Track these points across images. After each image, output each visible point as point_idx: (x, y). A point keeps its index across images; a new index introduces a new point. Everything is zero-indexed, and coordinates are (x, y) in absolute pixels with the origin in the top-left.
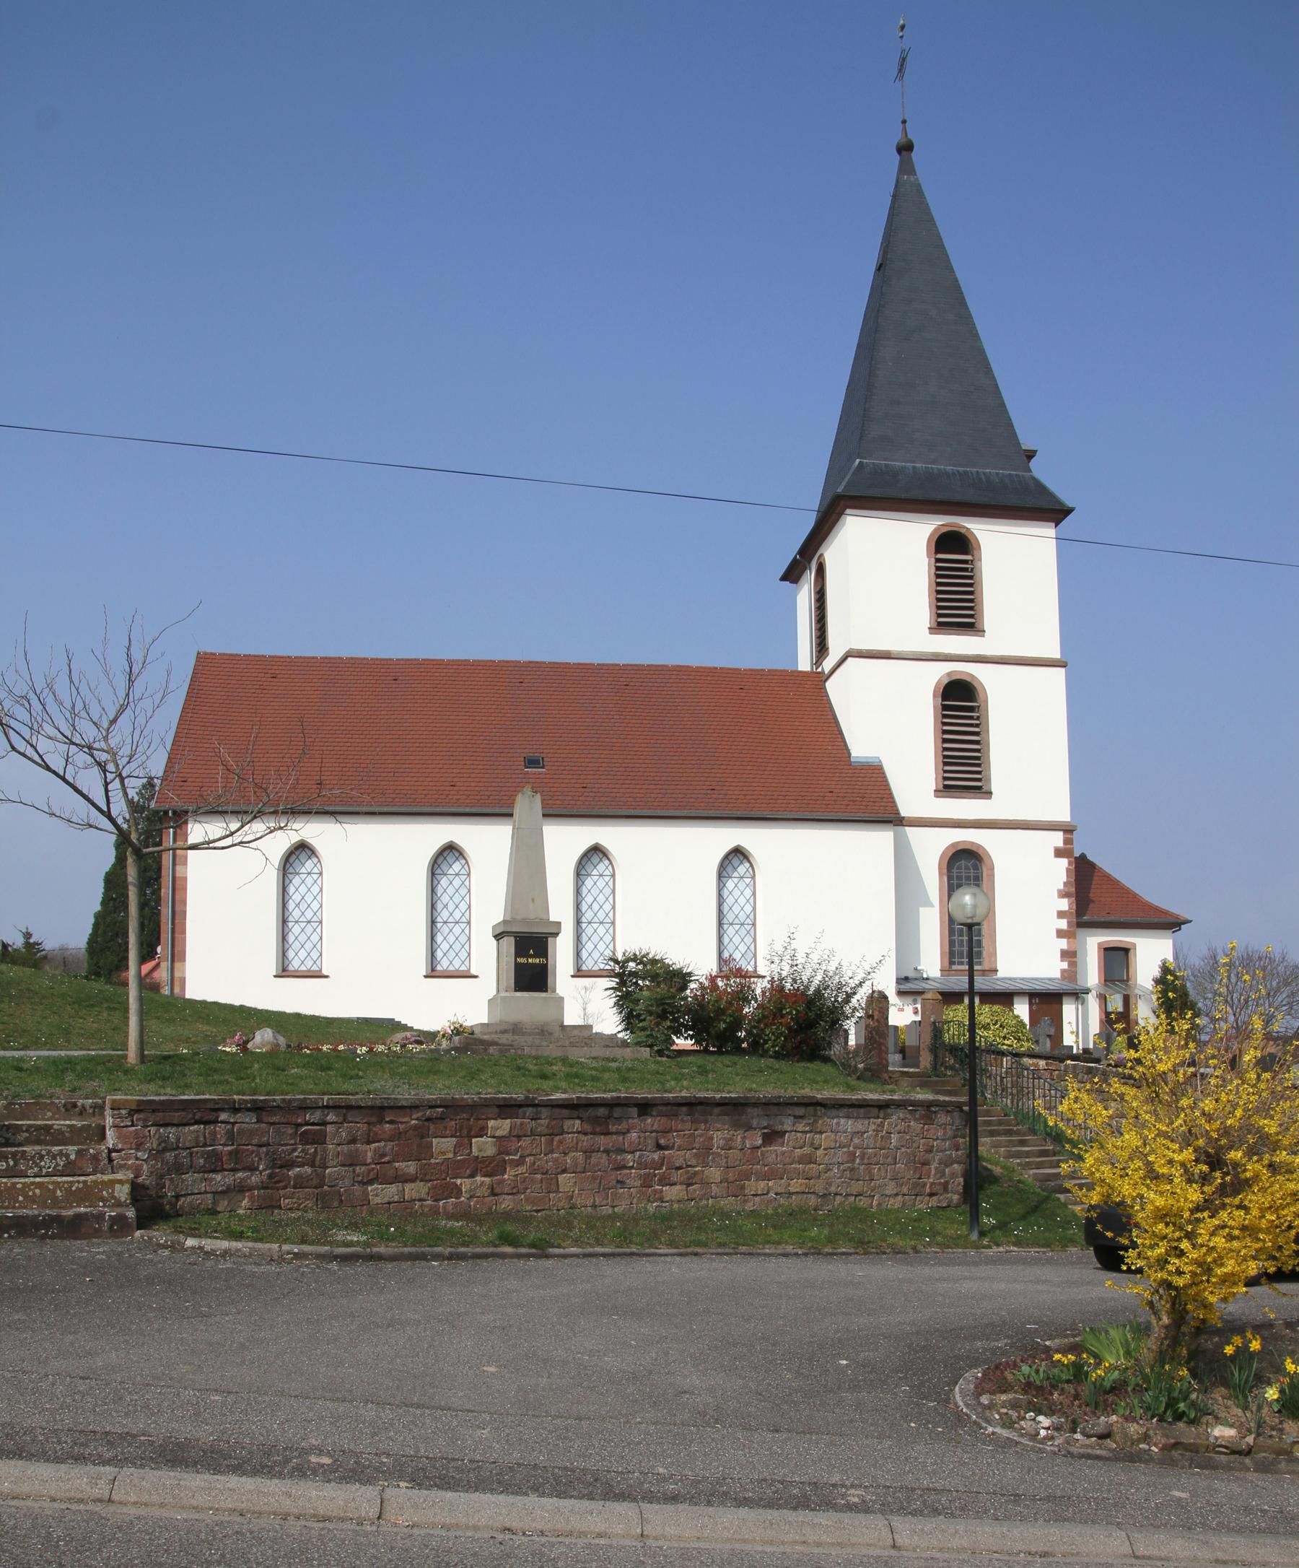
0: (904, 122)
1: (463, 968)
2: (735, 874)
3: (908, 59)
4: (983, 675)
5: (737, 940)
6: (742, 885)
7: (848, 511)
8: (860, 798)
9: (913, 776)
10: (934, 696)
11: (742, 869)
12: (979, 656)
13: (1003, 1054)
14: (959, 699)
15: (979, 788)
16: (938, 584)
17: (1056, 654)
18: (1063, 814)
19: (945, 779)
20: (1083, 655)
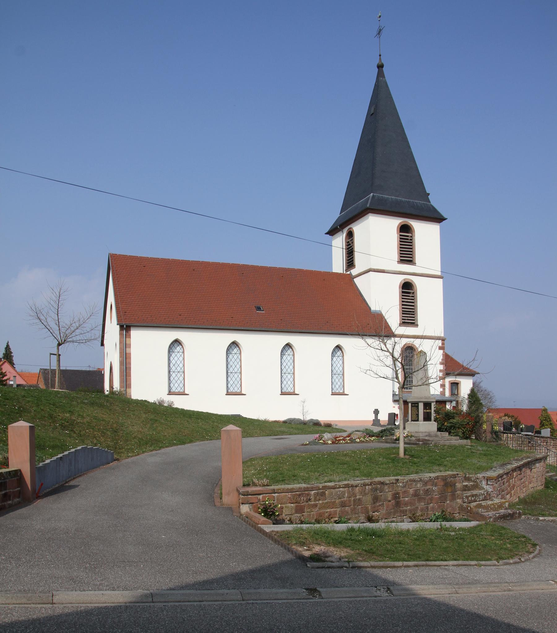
0: (380, 55)
1: (341, 391)
3: (383, 31)
4: (415, 280)
5: (337, 380)
6: (338, 359)
8: (372, 326)
9: (393, 318)
14: (407, 288)
15: (414, 323)
16: (401, 245)
17: (439, 273)
18: (440, 332)
19: (403, 319)
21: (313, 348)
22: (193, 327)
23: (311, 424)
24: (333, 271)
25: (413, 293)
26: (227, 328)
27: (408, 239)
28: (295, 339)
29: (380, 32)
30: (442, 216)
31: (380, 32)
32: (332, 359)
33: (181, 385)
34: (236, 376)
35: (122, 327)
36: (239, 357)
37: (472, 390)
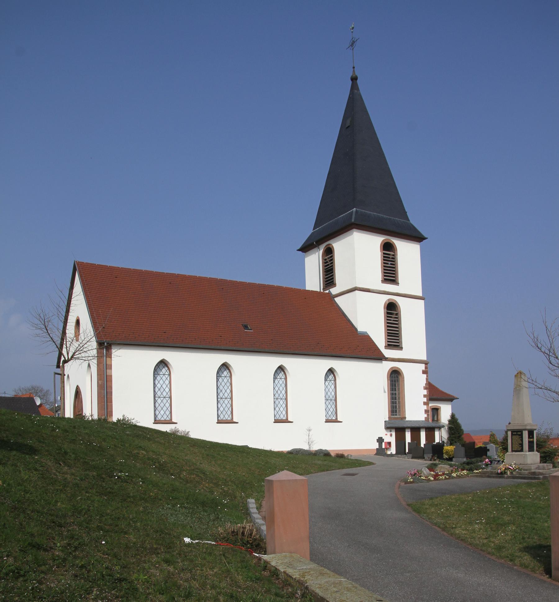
0: (354, 68)
1: (334, 418)
4: (400, 301)
6: (331, 384)
11: (226, 373)
12: (384, 291)
14: (392, 309)
17: (420, 294)
19: (388, 342)
20: (432, 294)
21: (308, 371)
22: (181, 346)
23: (322, 455)
24: (307, 289)
25: (397, 314)
26: (218, 347)
27: (389, 258)
28: (288, 362)
29: (353, 44)
30: (423, 236)
31: (353, 44)
32: (155, 379)
33: (168, 413)
34: (226, 402)
35: (100, 344)
36: (229, 380)
37: (453, 416)
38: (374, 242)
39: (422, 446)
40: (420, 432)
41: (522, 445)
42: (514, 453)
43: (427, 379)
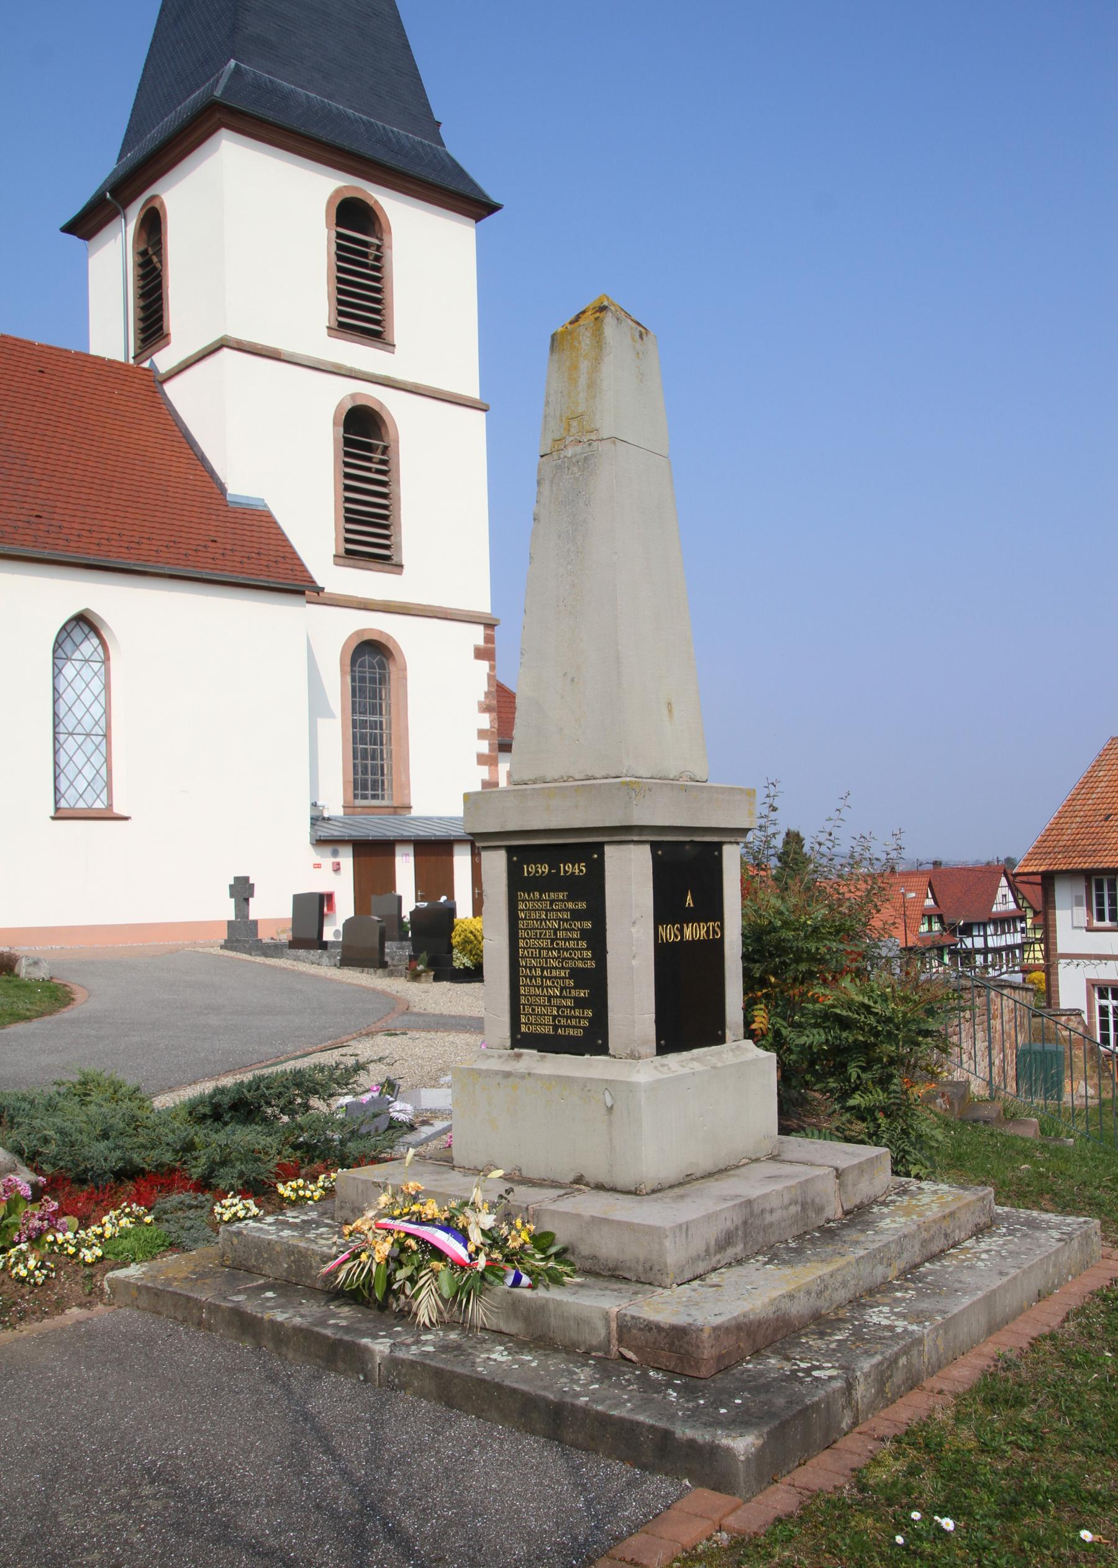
1: (99, 805)
2: (77, 655)
4: (397, 408)
5: (79, 759)
6: (87, 673)
7: (224, 132)
9: (312, 526)
10: (335, 424)
12: (388, 378)
13: (1033, 943)
14: (363, 430)
15: (387, 558)
19: (347, 541)
24: (92, 352)
25: (385, 450)
38: (305, 191)
39: (426, 904)
40: (451, 855)
41: (593, 984)
42: (531, 1060)
43: (491, 678)
